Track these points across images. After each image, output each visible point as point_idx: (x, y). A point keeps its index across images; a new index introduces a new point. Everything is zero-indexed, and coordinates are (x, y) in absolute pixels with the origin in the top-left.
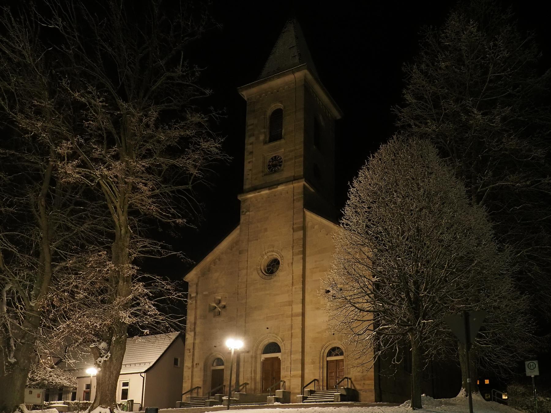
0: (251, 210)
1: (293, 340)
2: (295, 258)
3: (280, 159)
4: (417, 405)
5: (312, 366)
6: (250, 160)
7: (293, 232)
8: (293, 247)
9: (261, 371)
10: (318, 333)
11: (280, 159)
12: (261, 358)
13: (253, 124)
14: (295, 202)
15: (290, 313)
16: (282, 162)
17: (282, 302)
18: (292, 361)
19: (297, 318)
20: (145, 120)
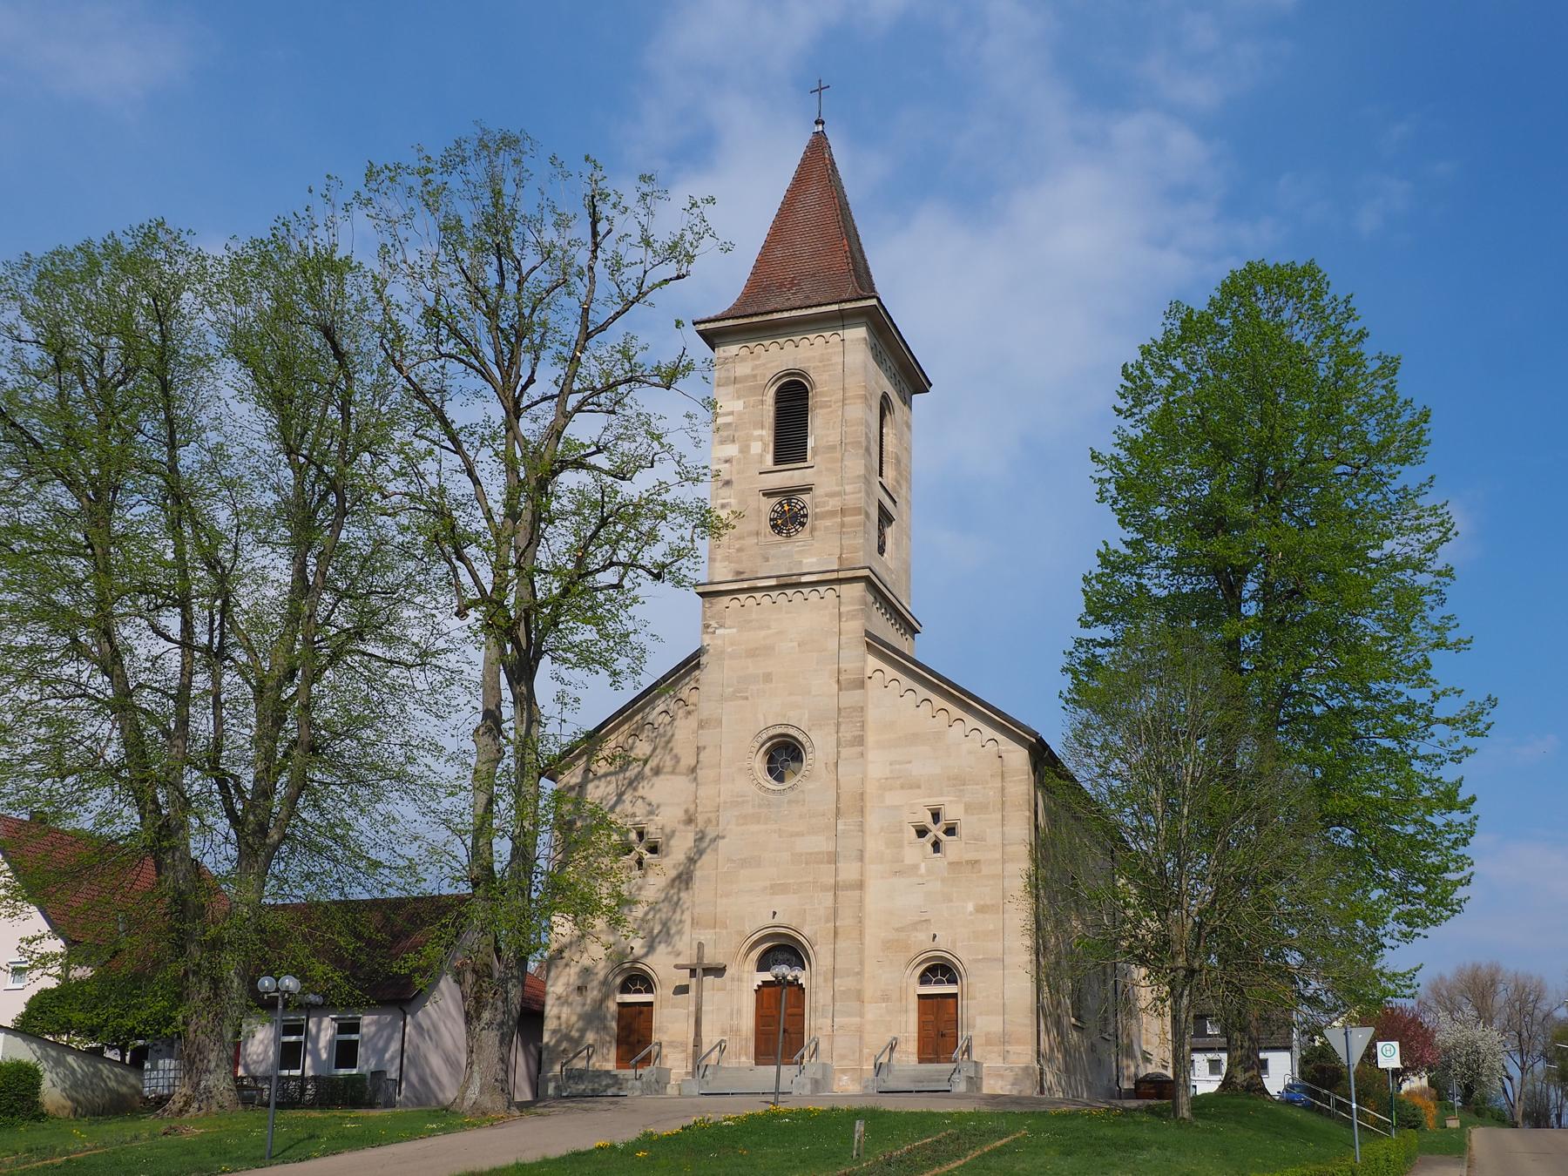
0: (728, 623)
1: (841, 944)
2: (845, 752)
3: (802, 508)
4: (1390, 367)
5: (884, 1005)
6: (724, 501)
7: (840, 689)
8: (838, 725)
9: (1032, 992)
10: (897, 930)
11: (802, 508)
12: (752, 980)
13: (731, 413)
14: (843, 619)
15: (832, 881)
16: (806, 516)
17: (811, 854)
18: (837, 994)
19: (849, 893)
20: (282, 220)
